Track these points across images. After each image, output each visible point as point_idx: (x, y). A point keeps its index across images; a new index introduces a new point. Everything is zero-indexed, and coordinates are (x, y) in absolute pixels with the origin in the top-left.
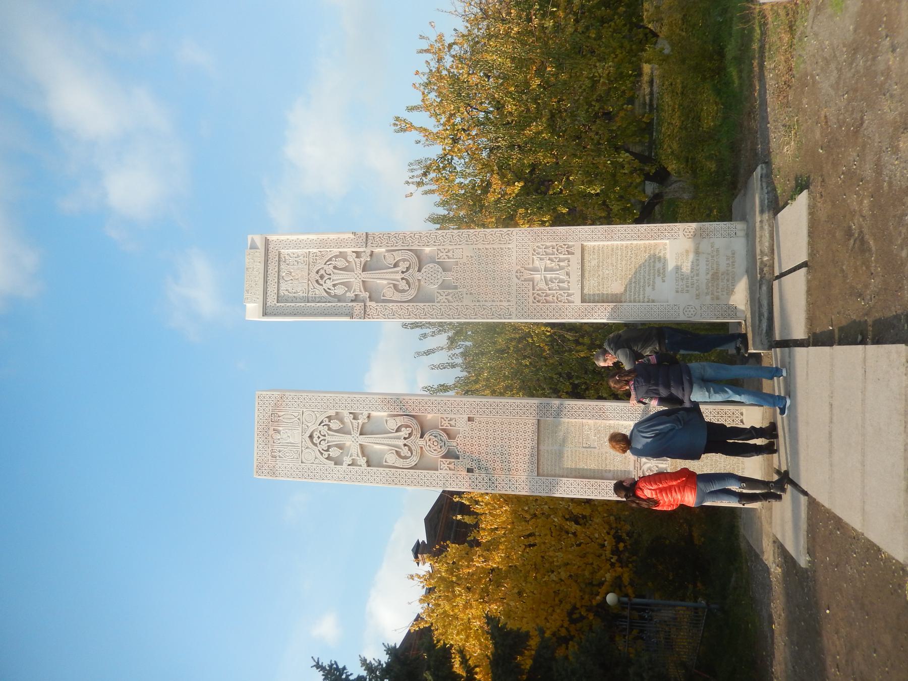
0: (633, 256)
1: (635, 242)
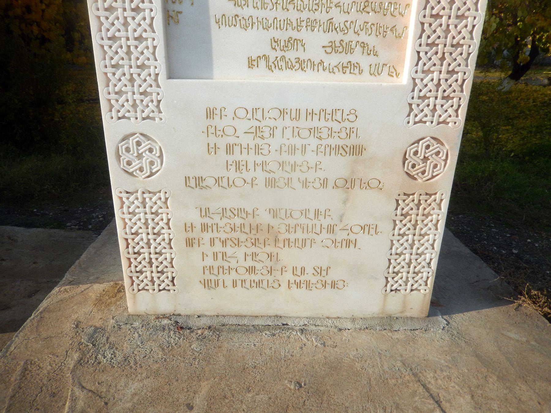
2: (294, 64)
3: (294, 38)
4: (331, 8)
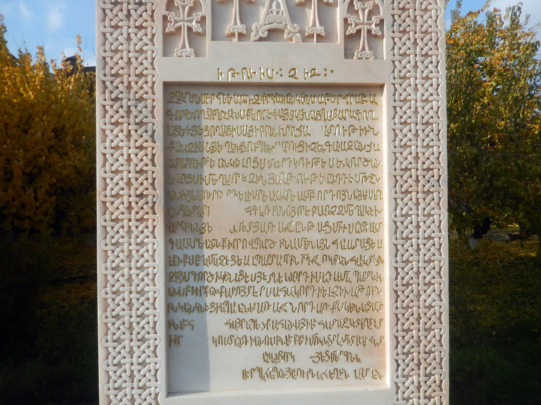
0: (339, 268)
1: (387, 272)
2: (285, 373)
3: (284, 351)
4: (315, 325)
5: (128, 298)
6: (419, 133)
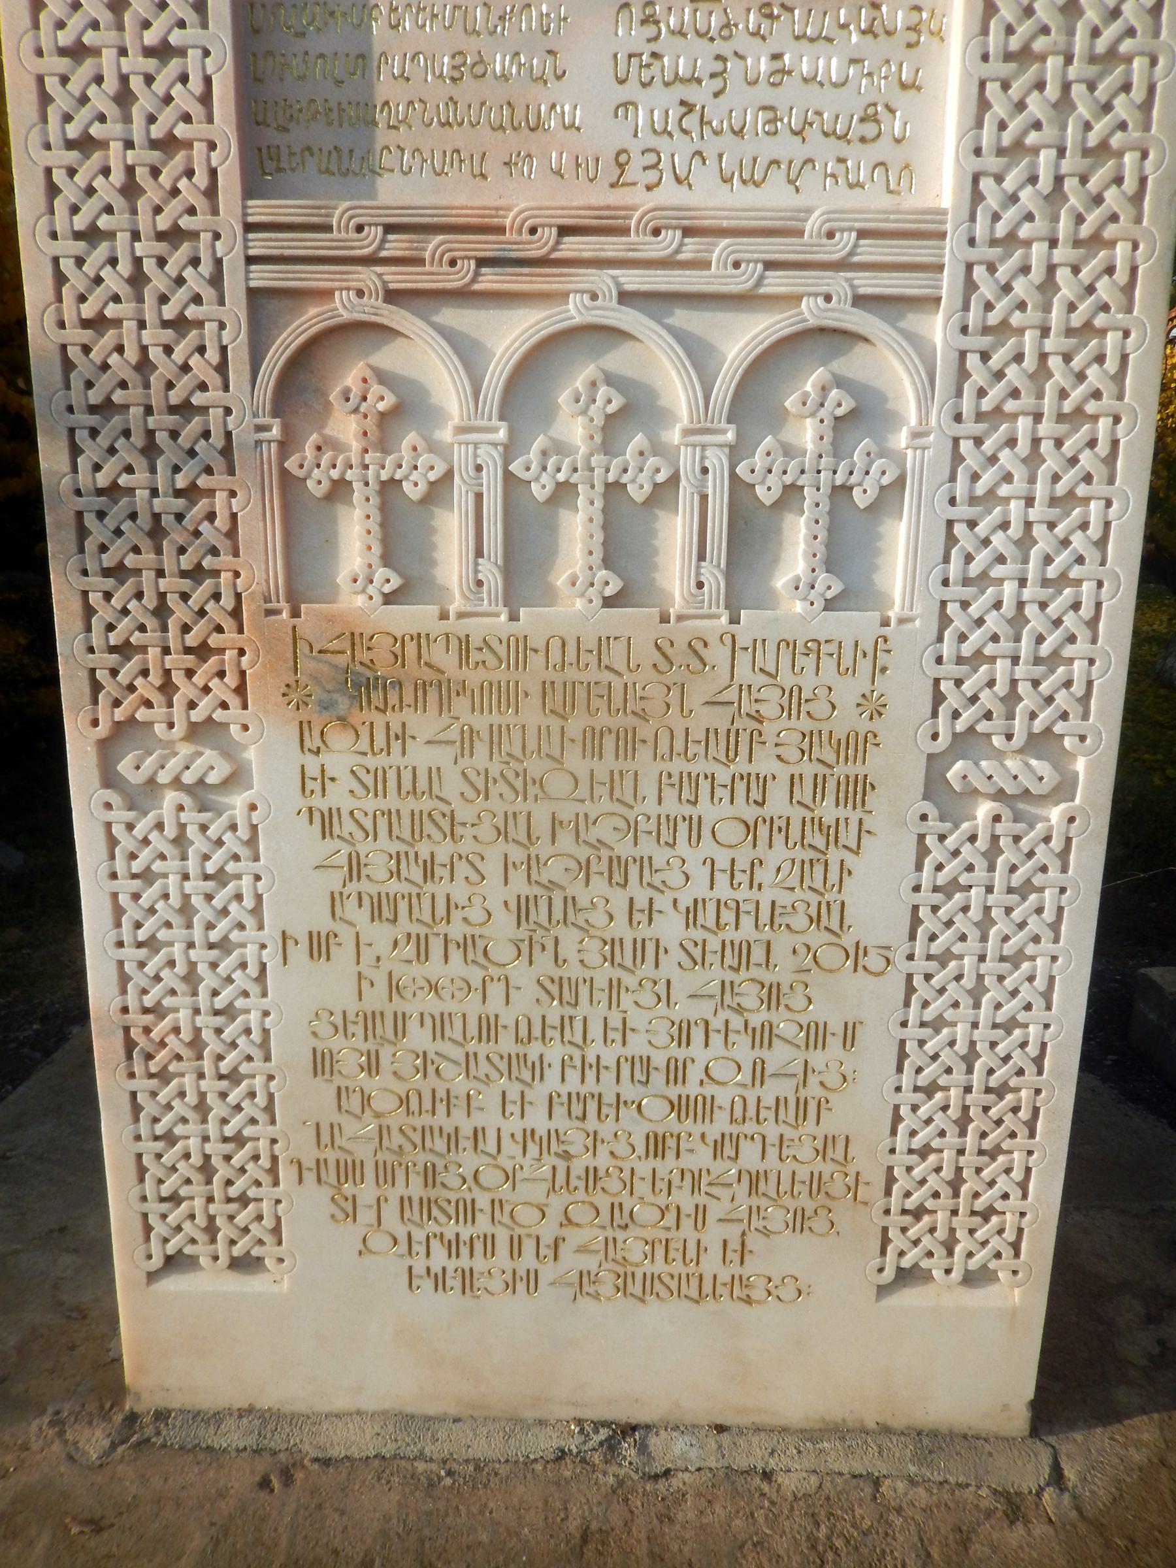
5: (190, 1028)
6: (1020, 690)
